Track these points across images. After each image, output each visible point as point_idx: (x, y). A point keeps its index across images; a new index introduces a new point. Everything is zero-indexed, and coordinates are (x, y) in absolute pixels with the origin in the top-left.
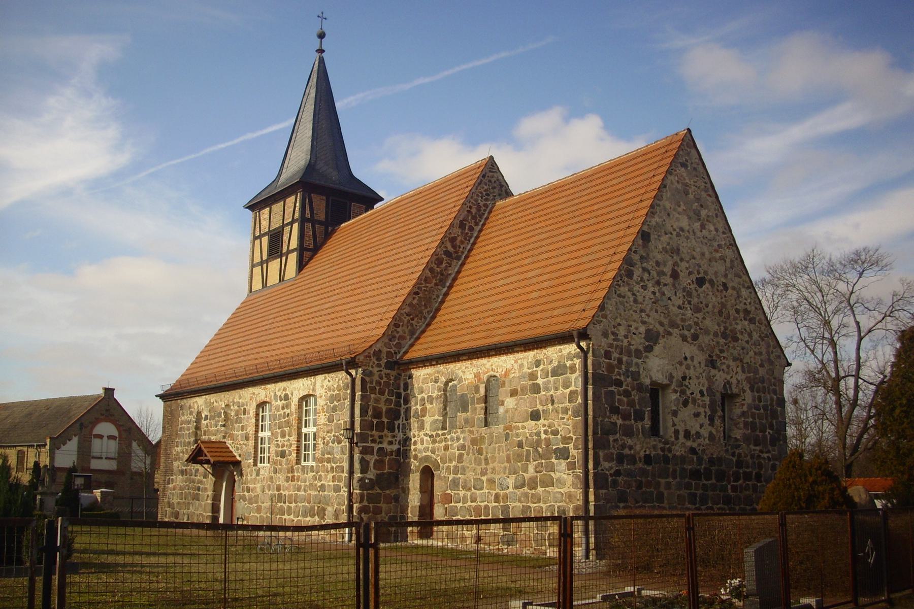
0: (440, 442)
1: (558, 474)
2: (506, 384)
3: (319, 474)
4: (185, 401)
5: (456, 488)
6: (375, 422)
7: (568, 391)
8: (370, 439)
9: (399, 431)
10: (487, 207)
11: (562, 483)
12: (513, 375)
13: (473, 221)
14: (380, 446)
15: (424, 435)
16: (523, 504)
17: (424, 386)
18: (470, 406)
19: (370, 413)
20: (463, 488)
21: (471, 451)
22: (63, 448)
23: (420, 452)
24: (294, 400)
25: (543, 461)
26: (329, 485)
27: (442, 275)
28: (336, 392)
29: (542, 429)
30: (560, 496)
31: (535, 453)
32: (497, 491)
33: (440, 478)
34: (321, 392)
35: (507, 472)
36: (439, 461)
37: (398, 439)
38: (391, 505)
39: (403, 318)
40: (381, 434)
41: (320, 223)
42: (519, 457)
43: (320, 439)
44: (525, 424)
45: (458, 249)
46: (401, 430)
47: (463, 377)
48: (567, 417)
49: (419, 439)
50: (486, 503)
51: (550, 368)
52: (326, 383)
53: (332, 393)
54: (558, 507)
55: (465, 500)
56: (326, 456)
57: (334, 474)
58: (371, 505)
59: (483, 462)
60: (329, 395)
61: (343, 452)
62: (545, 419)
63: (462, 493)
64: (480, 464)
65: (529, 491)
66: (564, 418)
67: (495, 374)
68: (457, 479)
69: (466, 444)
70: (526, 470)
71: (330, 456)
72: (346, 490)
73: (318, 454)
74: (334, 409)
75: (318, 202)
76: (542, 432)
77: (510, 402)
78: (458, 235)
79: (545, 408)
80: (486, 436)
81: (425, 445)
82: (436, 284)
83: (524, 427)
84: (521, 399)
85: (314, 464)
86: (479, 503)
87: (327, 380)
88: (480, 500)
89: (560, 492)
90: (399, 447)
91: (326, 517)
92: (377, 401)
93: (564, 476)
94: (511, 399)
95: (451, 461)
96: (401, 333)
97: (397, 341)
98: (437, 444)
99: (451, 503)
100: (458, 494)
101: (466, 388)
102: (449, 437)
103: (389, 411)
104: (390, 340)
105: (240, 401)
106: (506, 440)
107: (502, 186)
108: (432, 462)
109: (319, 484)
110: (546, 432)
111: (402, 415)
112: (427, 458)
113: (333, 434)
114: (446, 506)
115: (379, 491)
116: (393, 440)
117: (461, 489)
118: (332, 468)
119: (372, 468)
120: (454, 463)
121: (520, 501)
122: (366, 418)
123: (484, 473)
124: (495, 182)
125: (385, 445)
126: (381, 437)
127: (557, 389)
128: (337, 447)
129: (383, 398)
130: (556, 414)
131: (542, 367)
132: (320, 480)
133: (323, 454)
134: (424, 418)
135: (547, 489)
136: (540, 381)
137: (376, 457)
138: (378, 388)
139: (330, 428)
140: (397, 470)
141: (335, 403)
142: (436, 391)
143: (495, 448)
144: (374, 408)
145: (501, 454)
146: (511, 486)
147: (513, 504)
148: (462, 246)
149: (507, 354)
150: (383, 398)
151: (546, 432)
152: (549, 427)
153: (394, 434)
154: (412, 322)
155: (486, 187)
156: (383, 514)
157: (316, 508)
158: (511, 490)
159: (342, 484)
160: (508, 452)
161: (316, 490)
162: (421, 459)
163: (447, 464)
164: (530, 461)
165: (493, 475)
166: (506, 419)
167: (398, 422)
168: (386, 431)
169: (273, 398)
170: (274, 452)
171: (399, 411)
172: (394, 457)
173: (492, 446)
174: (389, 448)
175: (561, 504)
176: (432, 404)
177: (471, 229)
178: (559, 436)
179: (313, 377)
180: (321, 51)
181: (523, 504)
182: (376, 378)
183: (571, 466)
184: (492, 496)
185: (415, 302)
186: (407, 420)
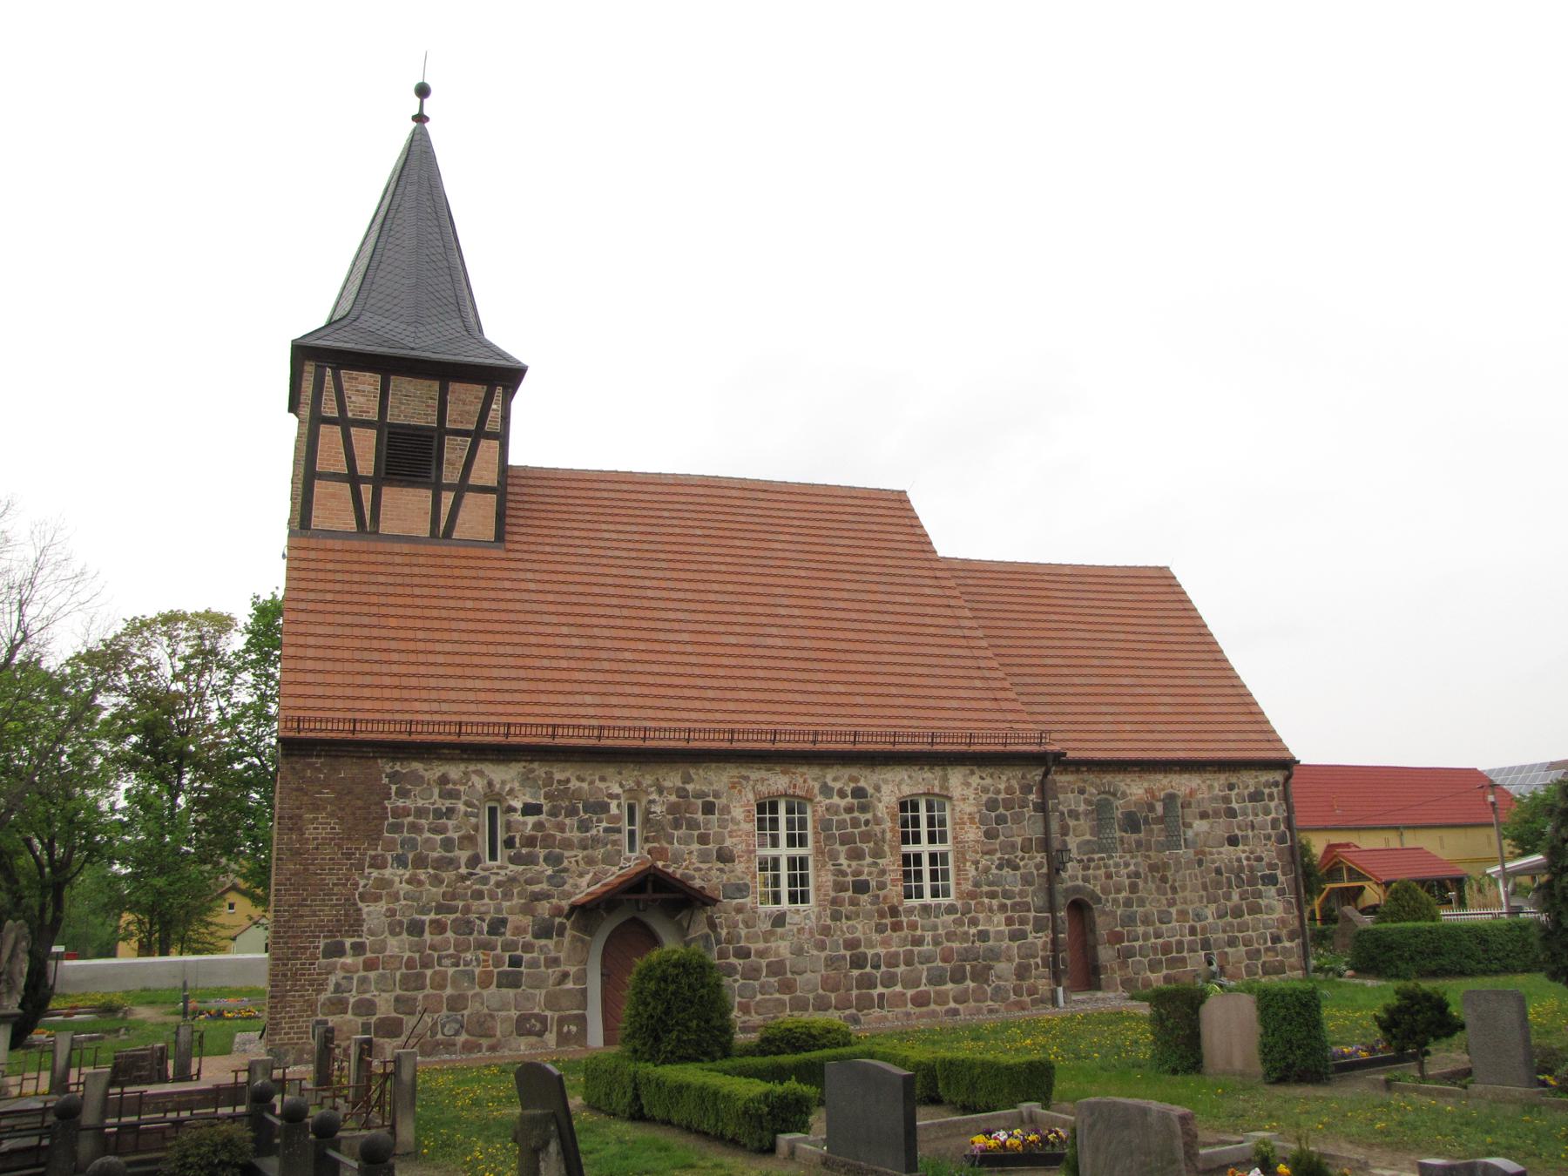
11: (1270, 909)
20: (1143, 922)
24: (885, 799)
29: (1243, 856)
32: (1192, 923)
33: (1104, 913)
36: (1099, 892)
42: (1218, 885)
43: (968, 864)
44: (1221, 849)
51: (1246, 792)
52: (975, 780)
55: (1146, 937)
56: (985, 889)
57: (1009, 913)
63: (1140, 930)
64: (1165, 894)
70: (1228, 897)
74: (1001, 820)
77: (1200, 826)
83: (1220, 853)
95: (1118, 891)
98: (1091, 871)
102: (1111, 862)
105: (690, 787)
109: (973, 931)
110: (1248, 859)
112: (1077, 889)
121: (1224, 931)
123: (1172, 903)
127: (1257, 815)
131: (1236, 791)
132: (974, 922)
133: (977, 884)
136: (1234, 805)
146: (1210, 916)
149: (1190, 772)
151: (1248, 859)
152: (1252, 853)
157: (968, 967)
158: (1210, 920)
163: (1113, 896)
169: (816, 791)
170: (830, 884)
180: (420, 118)
183: (1281, 892)
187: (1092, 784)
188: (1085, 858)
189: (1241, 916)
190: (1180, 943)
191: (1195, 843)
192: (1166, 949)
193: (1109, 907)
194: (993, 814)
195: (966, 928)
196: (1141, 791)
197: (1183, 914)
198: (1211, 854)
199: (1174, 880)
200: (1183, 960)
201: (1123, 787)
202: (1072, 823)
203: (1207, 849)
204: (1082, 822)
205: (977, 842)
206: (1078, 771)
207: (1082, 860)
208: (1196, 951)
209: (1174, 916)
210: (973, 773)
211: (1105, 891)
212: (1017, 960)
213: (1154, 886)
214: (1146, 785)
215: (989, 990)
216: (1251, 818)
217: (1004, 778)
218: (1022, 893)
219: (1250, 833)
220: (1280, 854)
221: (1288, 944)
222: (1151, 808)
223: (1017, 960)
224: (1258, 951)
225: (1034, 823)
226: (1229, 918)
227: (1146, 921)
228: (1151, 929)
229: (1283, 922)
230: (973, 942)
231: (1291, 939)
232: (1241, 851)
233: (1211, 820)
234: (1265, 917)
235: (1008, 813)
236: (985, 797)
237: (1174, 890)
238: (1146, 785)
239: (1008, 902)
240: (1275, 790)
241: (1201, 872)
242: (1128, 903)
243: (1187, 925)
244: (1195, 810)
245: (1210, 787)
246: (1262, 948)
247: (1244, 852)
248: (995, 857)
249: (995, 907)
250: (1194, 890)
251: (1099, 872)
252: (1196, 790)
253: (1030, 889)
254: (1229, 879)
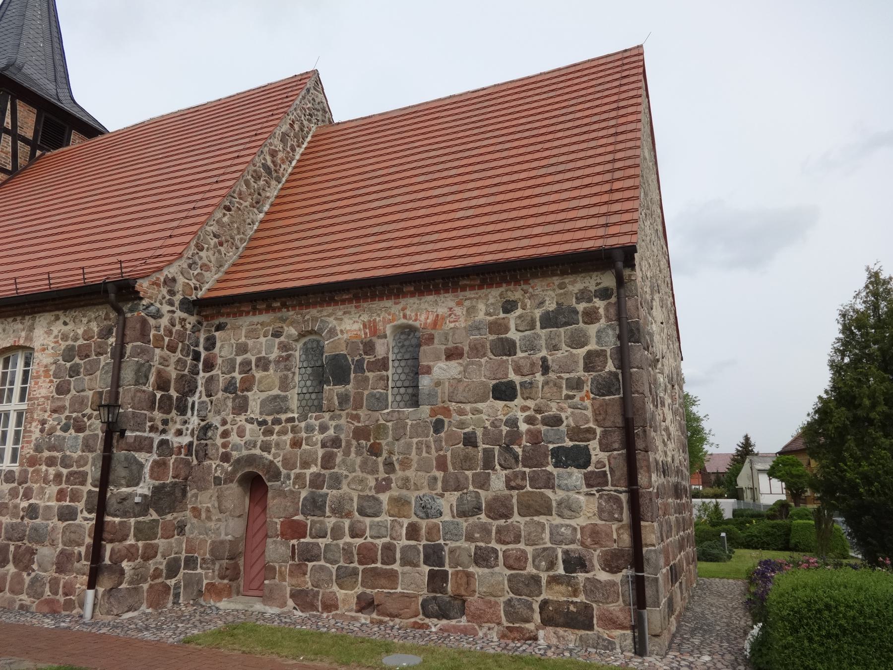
0: (283, 432)
1: (561, 494)
2: (436, 341)
3: (25, 486)
5: (318, 512)
6: (158, 396)
7: (582, 352)
8: (149, 424)
9: (192, 415)
10: (310, 130)
11: (568, 508)
12: (452, 325)
13: (295, 139)
14: (164, 437)
15: (246, 420)
16: (479, 544)
17: (250, 343)
18: (352, 376)
19: (152, 379)
20: (334, 511)
21: (353, 449)
22: (772, 463)
23: (236, 447)
25: (527, 470)
26: (48, 508)
27: (259, 194)
28: (81, 342)
29: (521, 416)
30: (569, 532)
31: (507, 456)
32: (414, 519)
33: (281, 493)
34: (45, 342)
35: (440, 484)
36: (279, 465)
37: (191, 427)
38: (173, 540)
39: (208, 238)
40: (165, 416)
41: (25, 140)
42: (466, 462)
43: (34, 424)
44: (480, 406)
45: (278, 167)
46: (196, 413)
47: (338, 328)
48: (579, 395)
49: (235, 427)
50: (387, 540)
51: (538, 313)
53: (70, 342)
54: (566, 552)
55: (337, 533)
56: (46, 454)
57: (64, 486)
58: (140, 544)
59: (381, 468)
60: (63, 347)
61: (88, 447)
62: (526, 399)
63: (330, 522)
64: (374, 471)
65: (490, 521)
66: (572, 397)
67: (411, 322)
68: (321, 496)
69: (342, 436)
70: (483, 483)
71: (55, 454)
72: (93, 515)
73: (28, 450)
74: (74, 371)
75: (25, 113)
76: (521, 419)
78: (280, 151)
79: (527, 379)
80: (390, 424)
81: (248, 437)
82: (252, 206)
84: (473, 364)
85: (16, 467)
86: (369, 540)
87: (61, 321)
88: (374, 533)
89: (570, 526)
90: (191, 439)
91: (35, 567)
92: (164, 361)
93: (577, 496)
94: (448, 363)
95: (306, 465)
96: (205, 260)
97: (199, 271)
98: (275, 437)
99: (304, 537)
100: (322, 523)
101: (345, 345)
102: (303, 424)
103: (180, 378)
104: (190, 266)
106: (437, 430)
107: (325, 112)
108: (264, 466)
109: (25, 504)
110: (530, 420)
111: (200, 388)
112: (251, 460)
113: (67, 413)
114: (294, 542)
115: (155, 516)
116: (184, 428)
117: (328, 514)
118: (58, 476)
119: (147, 476)
120: (314, 469)
121: (470, 538)
122: (144, 388)
124: (319, 103)
125: (170, 437)
126: (165, 422)
127: (556, 348)
128: (76, 438)
129: (174, 358)
130: (555, 389)
131: (519, 312)
132: (27, 495)
133: (38, 449)
134: (249, 394)
135: (536, 518)
136: (513, 334)
137: (155, 457)
138: (167, 339)
139: (60, 404)
140: (186, 479)
141: (77, 360)
142: (276, 350)
143: (409, 446)
144: (159, 373)
145: (424, 454)
147: (452, 544)
148: (283, 166)
149: (437, 292)
150: (174, 358)
151: (530, 420)
152: (538, 411)
153: (186, 418)
154: (220, 248)
155: (309, 105)
156: (159, 556)
157: (12, 548)
158: (447, 517)
159: (80, 505)
160: (441, 453)
161: (15, 515)
162: (238, 461)
164: (493, 469)
165: (404, 492)
166: (436, 395)
167: (193, 399)
168: (174, 412)
171: (196, 381)
172: (182, 456)
173: (402, 441)
174: (176, 441)
175: (572, 547)
176: (266, 369)
177: (293, 149)
178: (563, 428)
179: (27, 318)
181: (478, 544)
182: (164, 322)
183: (595, 481)
184: (402, 526)
185: (225, 220)
186: (209, 395)
187: (291, 324)
188: (269, 419)
189: (507, 516)
190: (389, 549)
191: (432, 395)
192: (366, 554)
193: (289, 486)
194: (68, 365)
195: (18, 501)
196: (357, 326)
197: (400, 503)
198: (461, 412)
199: (391, 453)
200: (392, 577)
201: (332, 322)
202: (258, 374)
203: (453, 406)
204: (271, 371)
205: (47, 398)
206: (269, 309)
207: (264, 423)
208: (416, 565)
209: (385, 506)
210: (57, 318)
211: (288, 463)
212: (61, 546)
213: (359, 460)
214: (365, 318)
215: (27, 579)
216: (544, 353)
217: (85, 320)
218: (82, 461)
219: (539, 378)
220: (600, 414)
221: (603, 576)
222: (369, 347)
223: (61, 546)
224: (536, 579)
225: (107, 372)
226: (483, 518)
227: (339, 510)
228: (347, 523)
229: (595, 534)
230: (22, 518)
231: (610, 566)
232: (517, 408)
233: (465, 360)
234: (557, 521)
235: (82, 362)
236: (63, 345)
237: (389, 466)
238: (365, 318)
239: (65, 471)
240: (600, 304)
241: (438, 441)
242: (317, 482)
243: (406, 522)
244: (439, 346)
245: (471, 311)
246: (544, 576)
247: (524, 409)
248: (63, 417)
249: (51, 477)
250: (424, 467)
251: (284, 438)
252: (443, 318)
253: (91, 456)
254: (488, 454)
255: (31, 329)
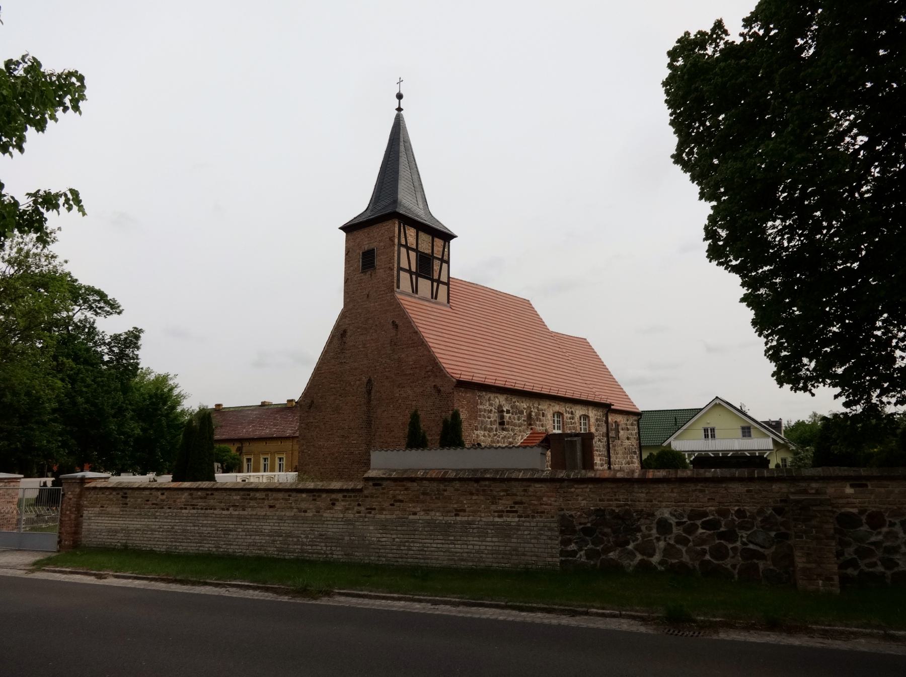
4: (484, 393)
74: (598, 425)
105: (540, 407)
180: (399, 109)
255: (588, 410)
